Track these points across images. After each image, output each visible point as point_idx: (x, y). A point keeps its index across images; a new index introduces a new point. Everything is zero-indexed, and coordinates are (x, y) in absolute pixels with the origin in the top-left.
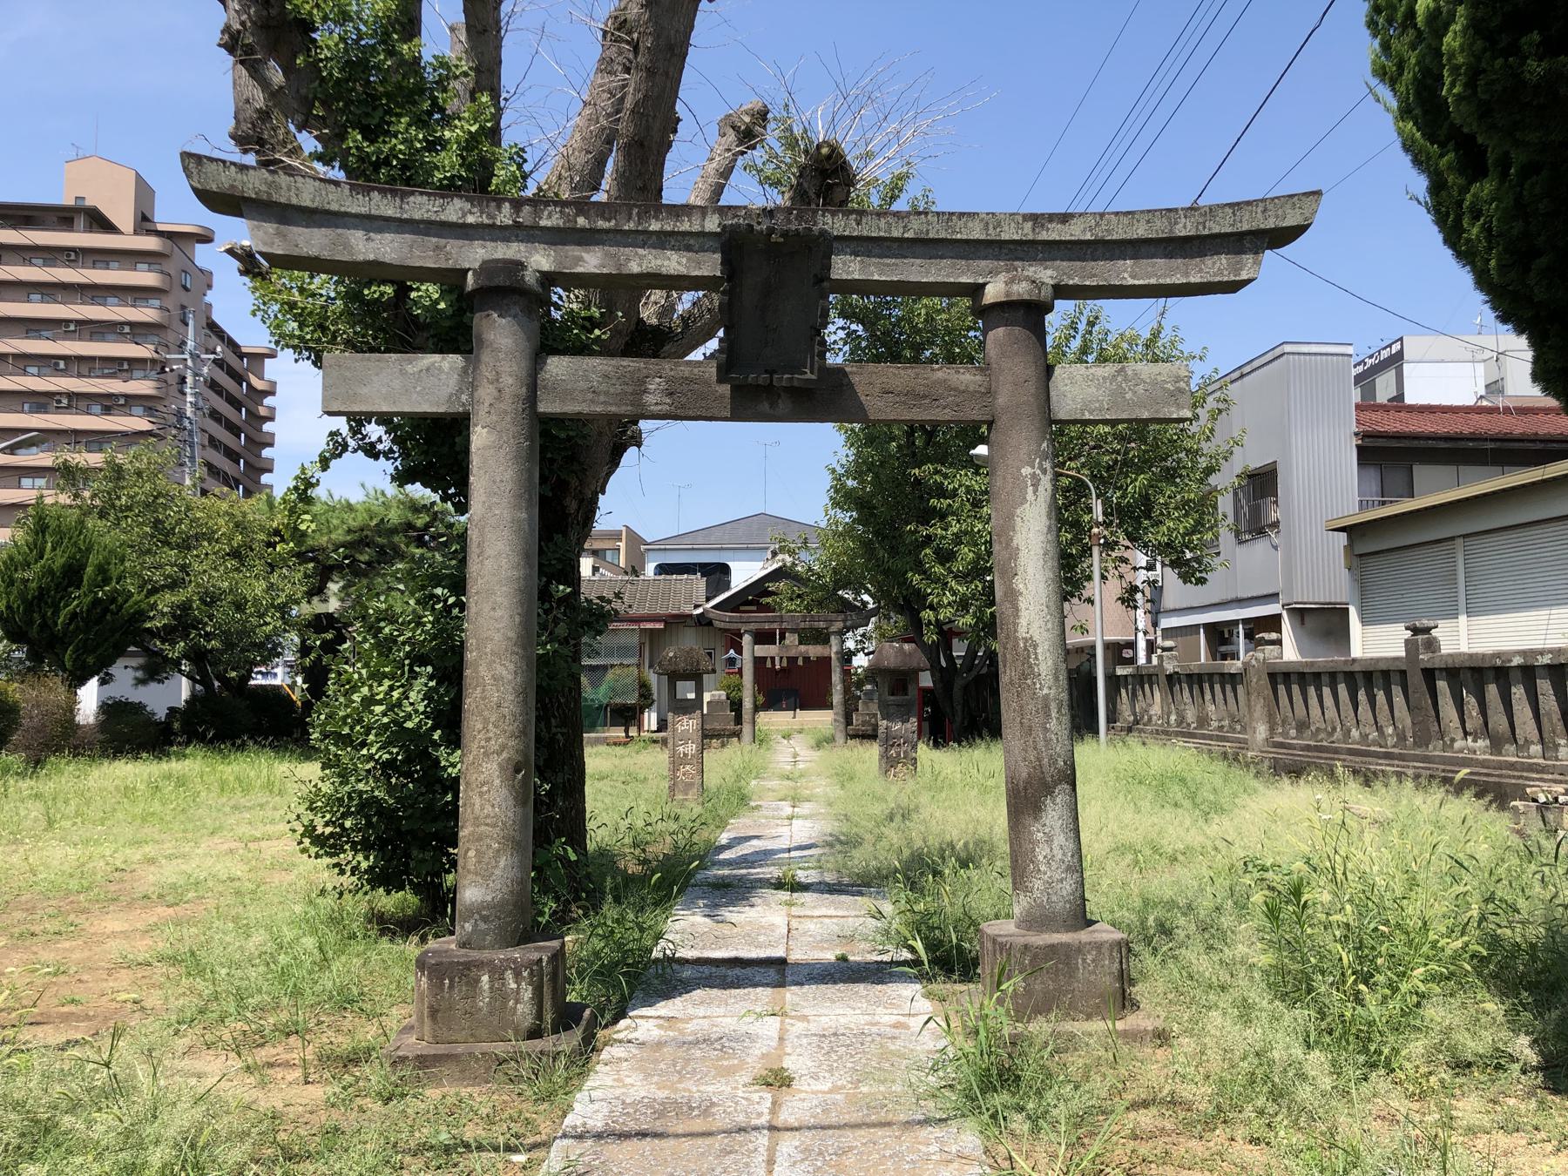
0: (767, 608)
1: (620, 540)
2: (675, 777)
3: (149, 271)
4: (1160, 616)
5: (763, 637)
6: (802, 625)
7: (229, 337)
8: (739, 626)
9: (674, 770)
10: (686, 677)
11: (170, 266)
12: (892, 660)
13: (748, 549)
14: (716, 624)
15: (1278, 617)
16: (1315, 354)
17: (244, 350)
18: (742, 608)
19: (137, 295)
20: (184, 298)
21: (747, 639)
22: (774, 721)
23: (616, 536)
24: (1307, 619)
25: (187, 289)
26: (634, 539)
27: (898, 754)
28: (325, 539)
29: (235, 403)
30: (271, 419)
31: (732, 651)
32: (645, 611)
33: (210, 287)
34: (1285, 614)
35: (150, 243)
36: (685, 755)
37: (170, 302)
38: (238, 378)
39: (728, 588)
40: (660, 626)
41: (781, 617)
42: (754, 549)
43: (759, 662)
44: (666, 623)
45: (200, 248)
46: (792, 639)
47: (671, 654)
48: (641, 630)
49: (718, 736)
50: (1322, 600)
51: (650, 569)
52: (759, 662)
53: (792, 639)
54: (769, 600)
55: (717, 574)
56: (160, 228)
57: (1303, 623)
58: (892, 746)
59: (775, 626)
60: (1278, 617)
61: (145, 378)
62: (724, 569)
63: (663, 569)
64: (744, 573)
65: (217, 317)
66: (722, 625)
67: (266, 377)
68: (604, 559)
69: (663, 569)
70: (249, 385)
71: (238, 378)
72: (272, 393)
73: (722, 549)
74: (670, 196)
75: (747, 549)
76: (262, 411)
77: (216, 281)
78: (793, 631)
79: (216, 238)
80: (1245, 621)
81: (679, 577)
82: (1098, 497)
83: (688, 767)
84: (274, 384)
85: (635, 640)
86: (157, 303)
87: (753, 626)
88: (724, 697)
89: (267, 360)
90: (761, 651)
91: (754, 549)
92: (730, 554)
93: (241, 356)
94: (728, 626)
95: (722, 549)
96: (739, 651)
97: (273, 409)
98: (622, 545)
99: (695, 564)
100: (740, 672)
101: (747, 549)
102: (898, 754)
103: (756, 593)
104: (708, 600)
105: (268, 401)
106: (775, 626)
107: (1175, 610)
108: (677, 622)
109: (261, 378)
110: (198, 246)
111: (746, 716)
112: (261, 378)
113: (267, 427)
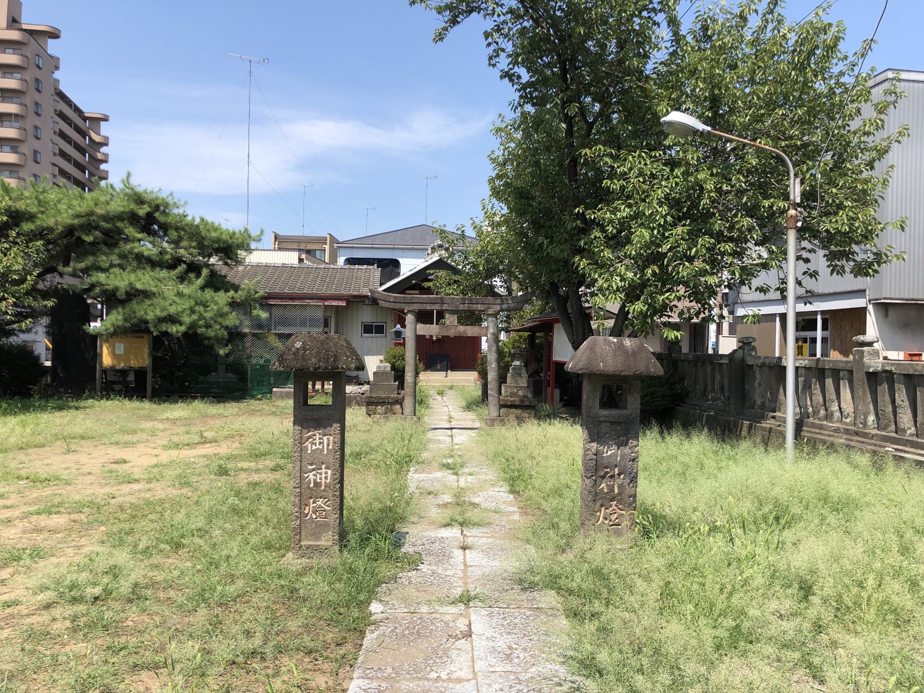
0: (428, 291)
1: (326, 244)
2: (302, 515)
3: (14, 54)
4: (736, 306)
5: (424, 317)
6: (461, 307)
7: (75, 106)
8: (403, 306)
9: (302, 504)
10: (323, 376)
11: (27, 51)
12: (610, 361)
13: (416, 250)
14: (381, 303)
15: (862, 312)
16: (913, 81)
17: (86, 115)
18: (407, 292)
19: (6, 70)
20: (38, 74)
21: (410, 318)
22: (431, 380)
23: (323, 241)
24: (891, 312)
25: (40, 68)
26: (333, 240)
27: (611, 489)
28: (53, 220)
29: (82, 151)
30: (106, 161)
31: (398, 326)
32: (332, 291)
33: (57, 68)
34: (870, 308)
35: (14, 35)
36: (317, 484)
37: (27, 76)
38: (83, 134)
39: (398, 274)
40: (343, 304)
41: (442, 299)
42: (418, 249)
43: (420, 339)
44: (348, 301)
45: (51, 42)
46: (451, 319)
47: (298, 345)
48: (326, 306)
49: (383, 403)
50: (906, 297)
51: (341, 261)
52: (420, 339)
53: (451, 319)
54: (430, 284)
55: (391, 266)
56: (24, 27)
57: (887, 316)
58: (603, 477)
59: (433, 307)
60: (862, 312)
61: (11, 127)
62: (395, 264)
63: (350, 261)
64: (409, 266)
65: (63, 88)
66: (387, 305)
67: (103, 132)
68: (315, 257)
69: (350, 261)
70: (90, 138)
71: (83, 134)
72: (106, 144)
73: (394, 248)
74: (423, 376)
75: (413, 249)
76: (99, 156)
77: (62, 65)
78: (452, 312)
79: (62, 35)
80: (823, 312)
81: (360, 267)
82: (796, 175)
83: (320, 502)
84: (107, 138)
85: (320, 314)
86: (19, 76)
87: (416, 307)
88: (389, 369)
89: (102, 123)
90: (424, 329)
91: (418, 249)
92: (400, 252)
93: (85, 119)
94: (392, 306)
95: (394, 248)
96: (404, 326)
97: (106, 155)
98: (327, 247)
99: (374, 259)
100: (403, 344)
101: (413, 249)
102: (611, 489)
103: (418, 281)
104: (381, 284)
105: (104, 149)
106: (433, 307)
107: (754, 302)
108: (355, 301)
109: (98, 134)
110: (50, 41)
111: (409, 377)
112: (98, 134)
113: (103, 167)
